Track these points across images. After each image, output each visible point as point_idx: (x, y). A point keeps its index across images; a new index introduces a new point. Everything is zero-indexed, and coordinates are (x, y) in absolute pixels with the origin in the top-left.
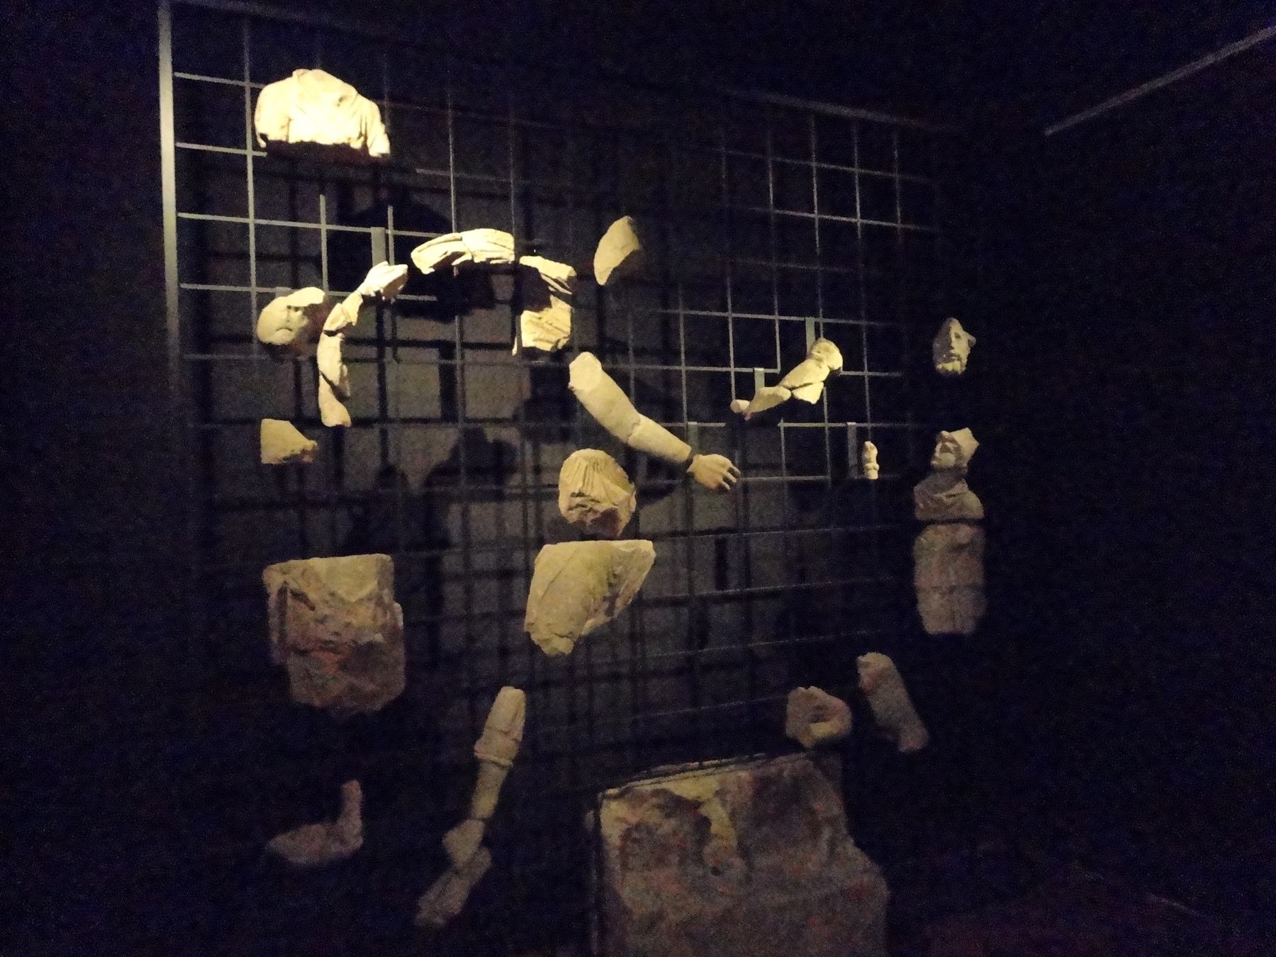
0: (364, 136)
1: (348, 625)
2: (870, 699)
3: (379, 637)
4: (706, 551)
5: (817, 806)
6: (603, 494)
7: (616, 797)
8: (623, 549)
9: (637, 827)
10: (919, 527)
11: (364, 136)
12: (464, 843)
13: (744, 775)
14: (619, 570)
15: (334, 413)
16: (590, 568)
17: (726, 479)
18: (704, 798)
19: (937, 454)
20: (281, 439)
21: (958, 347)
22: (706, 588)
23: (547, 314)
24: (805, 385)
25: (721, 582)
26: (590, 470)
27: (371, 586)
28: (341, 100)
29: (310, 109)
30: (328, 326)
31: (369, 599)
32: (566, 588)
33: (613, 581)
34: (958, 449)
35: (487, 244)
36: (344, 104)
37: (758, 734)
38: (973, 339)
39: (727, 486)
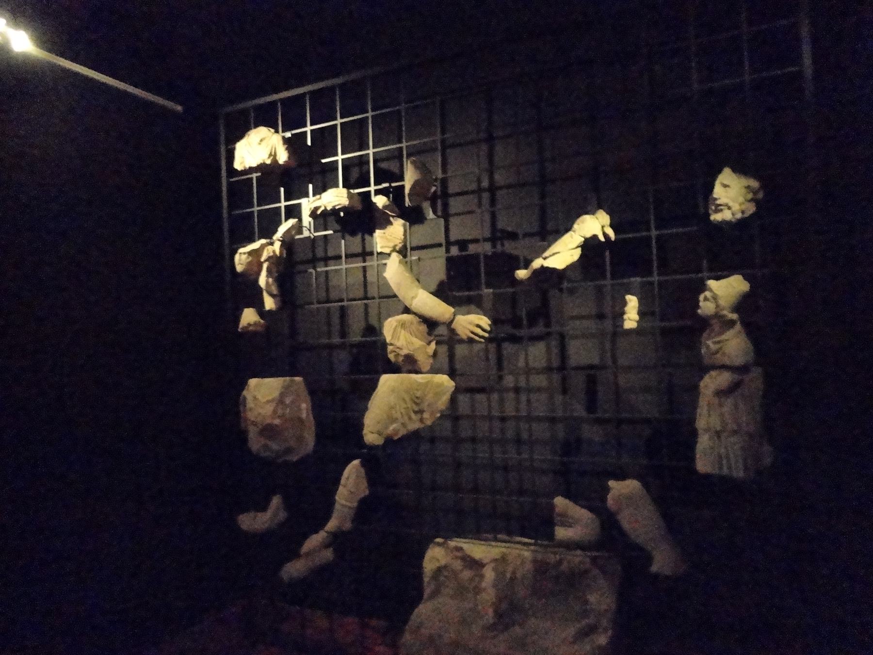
1: (260, 414)
2: (619, 517)
3: (277, 422)
4: (578, 381)
5: (592, 598)
6: (404, 343)
7: (439, 544)
8: (420, 381)
9: (445, 567)
10: (704, 370)
12: (315, 540)
13: (527, 554)
14: (418, 394)
16: (393, 391)
17: (473, 333)
18: (485, 561)
19: (701, 304)
21: (731, 196)
22: (579, 411)
23: (390, 229)
24: (554, 254)
25: (591, 405)
26: (399, 329)
27: (276, 394)
28: (261, 141)
30: (262, 260)
32: (389, 406)
33: (417, 401)
34: (715, 298)
36: (263, 143)
37: (538, 525)
38: (755, 184)
39: (477, 338)
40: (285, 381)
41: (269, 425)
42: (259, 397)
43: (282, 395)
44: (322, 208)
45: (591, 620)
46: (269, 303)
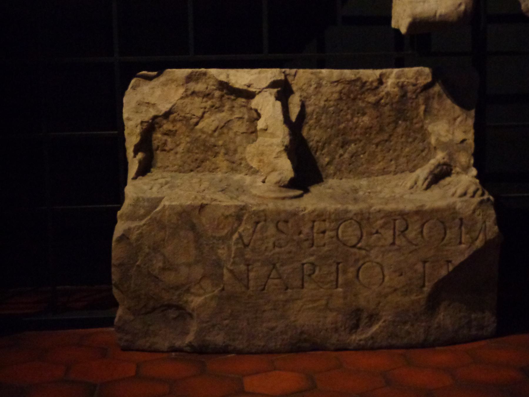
45: (440, 156)
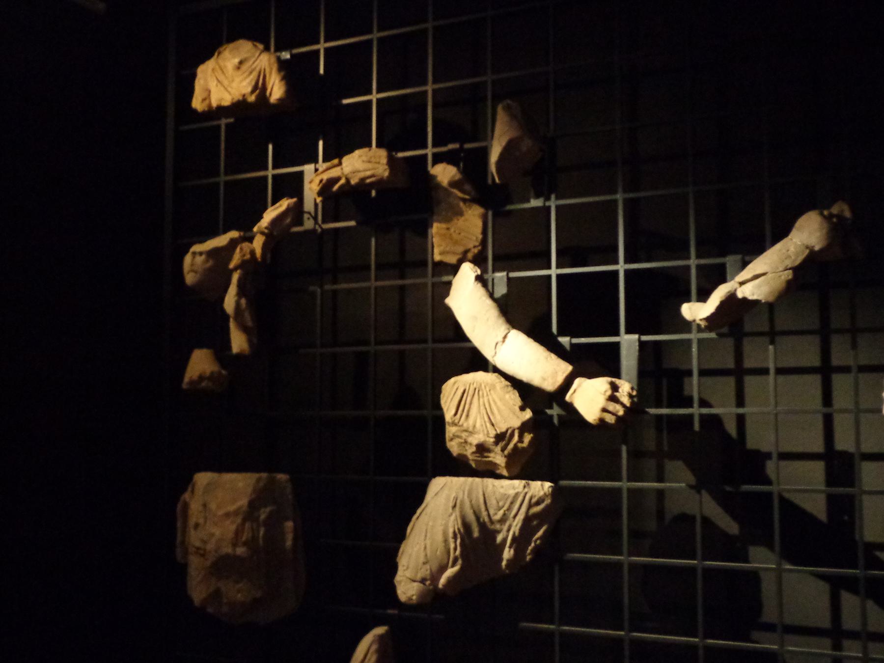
0: (260, 88)
11: (260, 88)
15: (238, 342)
20: (200, 363)
23: (460, 222)
28: (241, 63)
29: (229, 78)
31: (236, 513)
35: (363, 164)
40: (258, 480)
41: (227, 556)
42: (213, 506)
43: (253, 506)
44: (343, 181)
46: (238, 342)
